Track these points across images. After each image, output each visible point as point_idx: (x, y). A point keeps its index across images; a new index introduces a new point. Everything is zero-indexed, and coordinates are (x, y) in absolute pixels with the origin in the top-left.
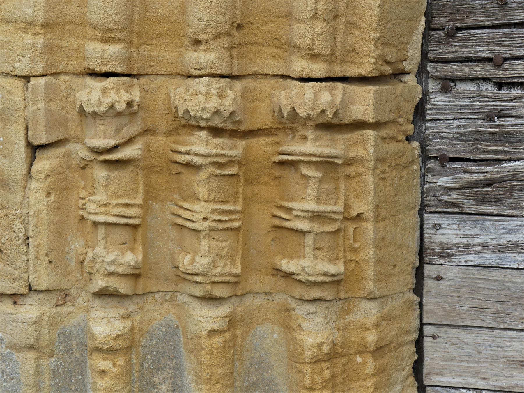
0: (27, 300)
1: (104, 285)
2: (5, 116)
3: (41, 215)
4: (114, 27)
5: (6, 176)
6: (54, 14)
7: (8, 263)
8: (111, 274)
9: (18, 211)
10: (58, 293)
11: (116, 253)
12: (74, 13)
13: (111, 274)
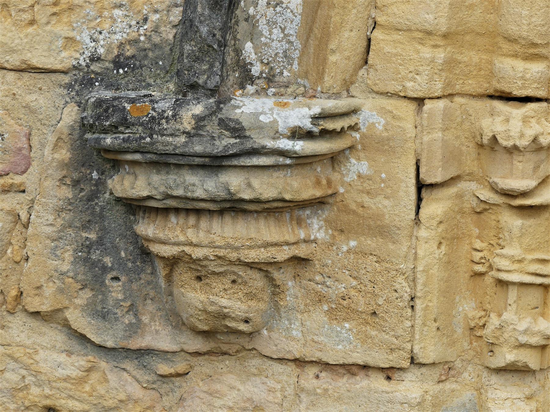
0: (406, 375)
1: (513, 360)
2: (390, 147)
3: (431, 271)
4: (539, 42)
5: (387, 221)
6: (455, 21)
7: (384, 329)
8: (522, 346)
9: (403, 265)
10: (441, 367)
11: (529, 319)
12: (476, 21)
13: (522, 346)
